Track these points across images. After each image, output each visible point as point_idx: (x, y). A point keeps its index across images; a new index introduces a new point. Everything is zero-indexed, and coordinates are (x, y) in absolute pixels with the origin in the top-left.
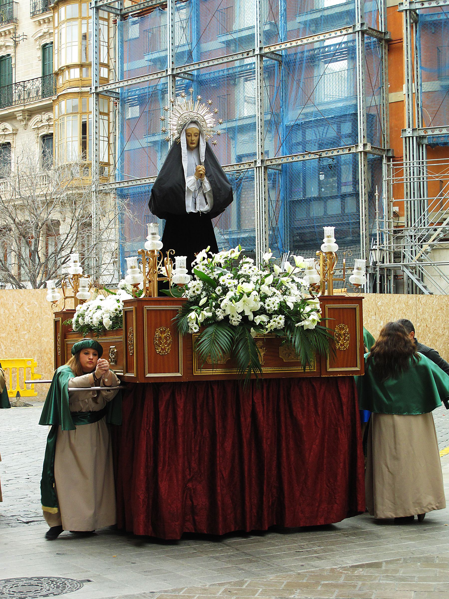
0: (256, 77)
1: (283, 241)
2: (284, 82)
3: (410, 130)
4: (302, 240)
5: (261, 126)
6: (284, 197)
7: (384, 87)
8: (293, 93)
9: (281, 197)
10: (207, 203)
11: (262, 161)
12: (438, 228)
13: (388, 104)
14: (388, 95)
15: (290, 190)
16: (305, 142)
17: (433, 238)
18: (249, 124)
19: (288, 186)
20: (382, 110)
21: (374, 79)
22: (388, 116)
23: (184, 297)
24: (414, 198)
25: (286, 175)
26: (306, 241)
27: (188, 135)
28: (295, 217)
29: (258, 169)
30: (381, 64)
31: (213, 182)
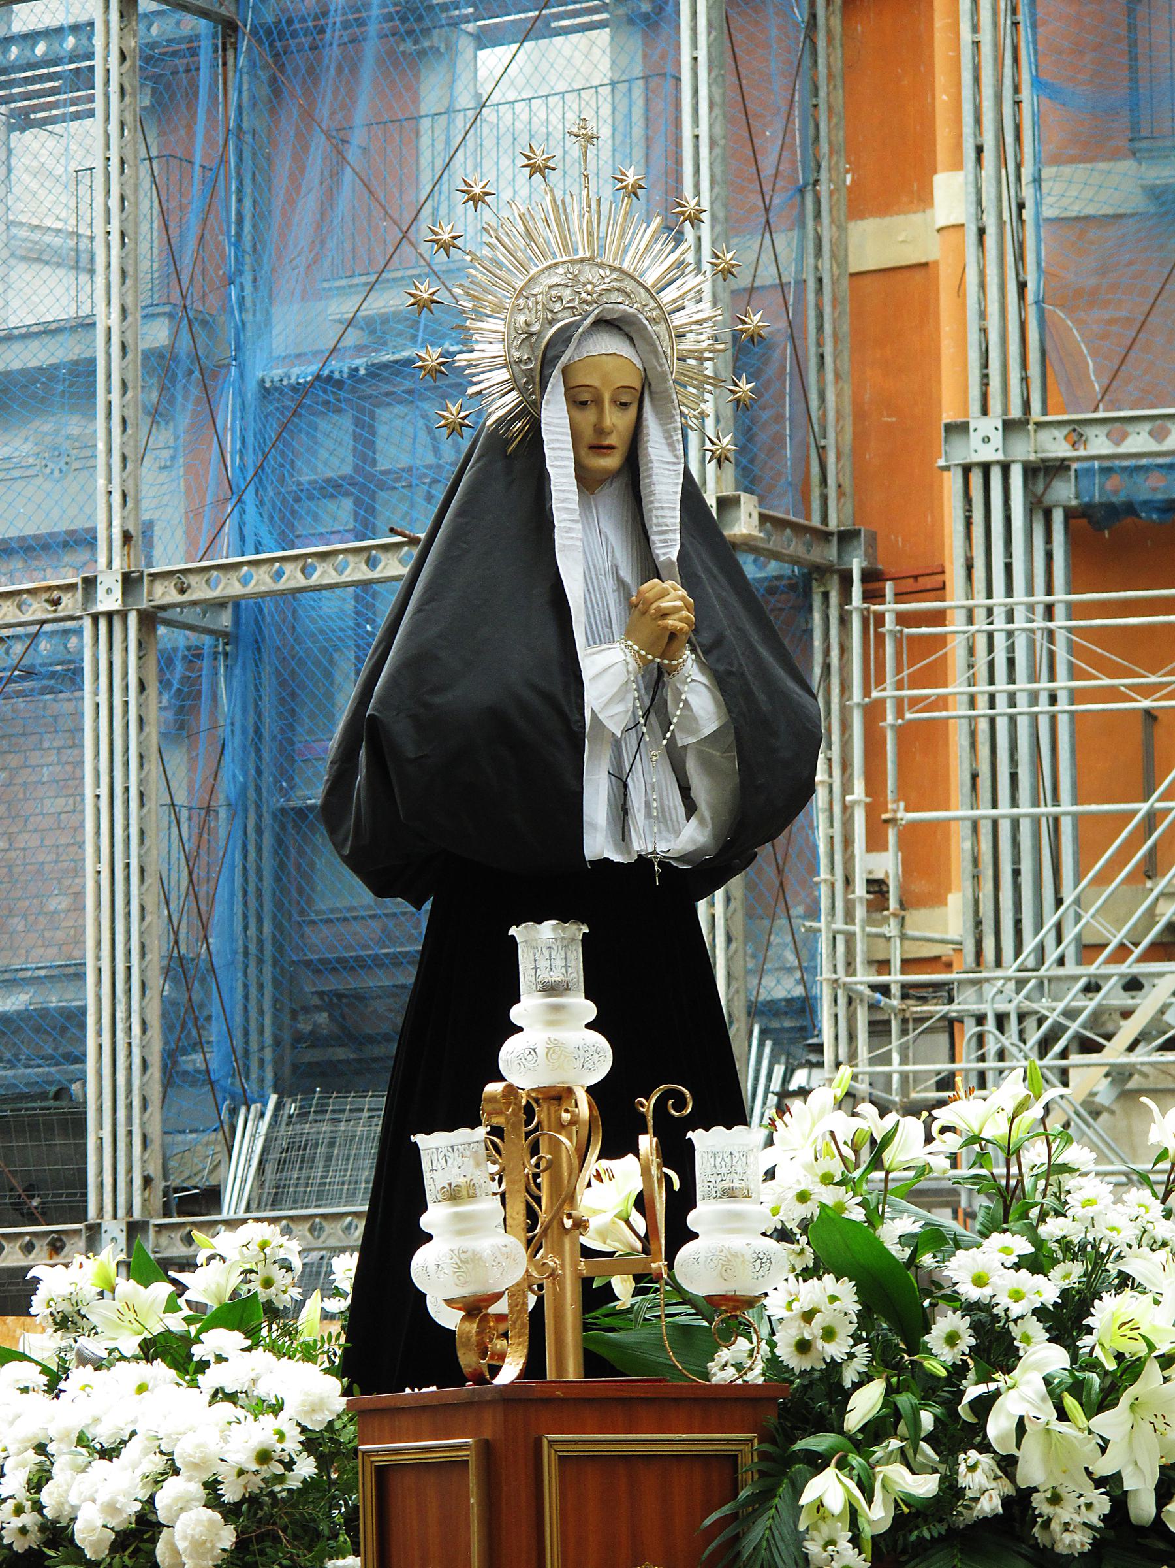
0: (99, 105)
1: (238, 1042)
2: (248, 138)
3: (988, 427)
4: (347, 1036)
5: (124, 385)
6: (244, 787)
7: (823, 188)
8: (308, 205)
9: (227, 788)
10: (691, 808)
11: (129, 582)
12: (1161, 975)
13: (845, 282)
14: (843, 229)
15: (282, 750)
16: (370, 477)
17: (1129, 1030)
18: (40, 369)
19: (270, 726)
20: (812, 313)
21: (770, 136)
22: (846, 346)
23: (730, 1373)
24: (1014, 803)
25: (258, 663)
26: (370, 1039)
27: (577, 400)
28: (310, 901)
29: (103, 624)
30: (807, 62)
31: (733, 681)
